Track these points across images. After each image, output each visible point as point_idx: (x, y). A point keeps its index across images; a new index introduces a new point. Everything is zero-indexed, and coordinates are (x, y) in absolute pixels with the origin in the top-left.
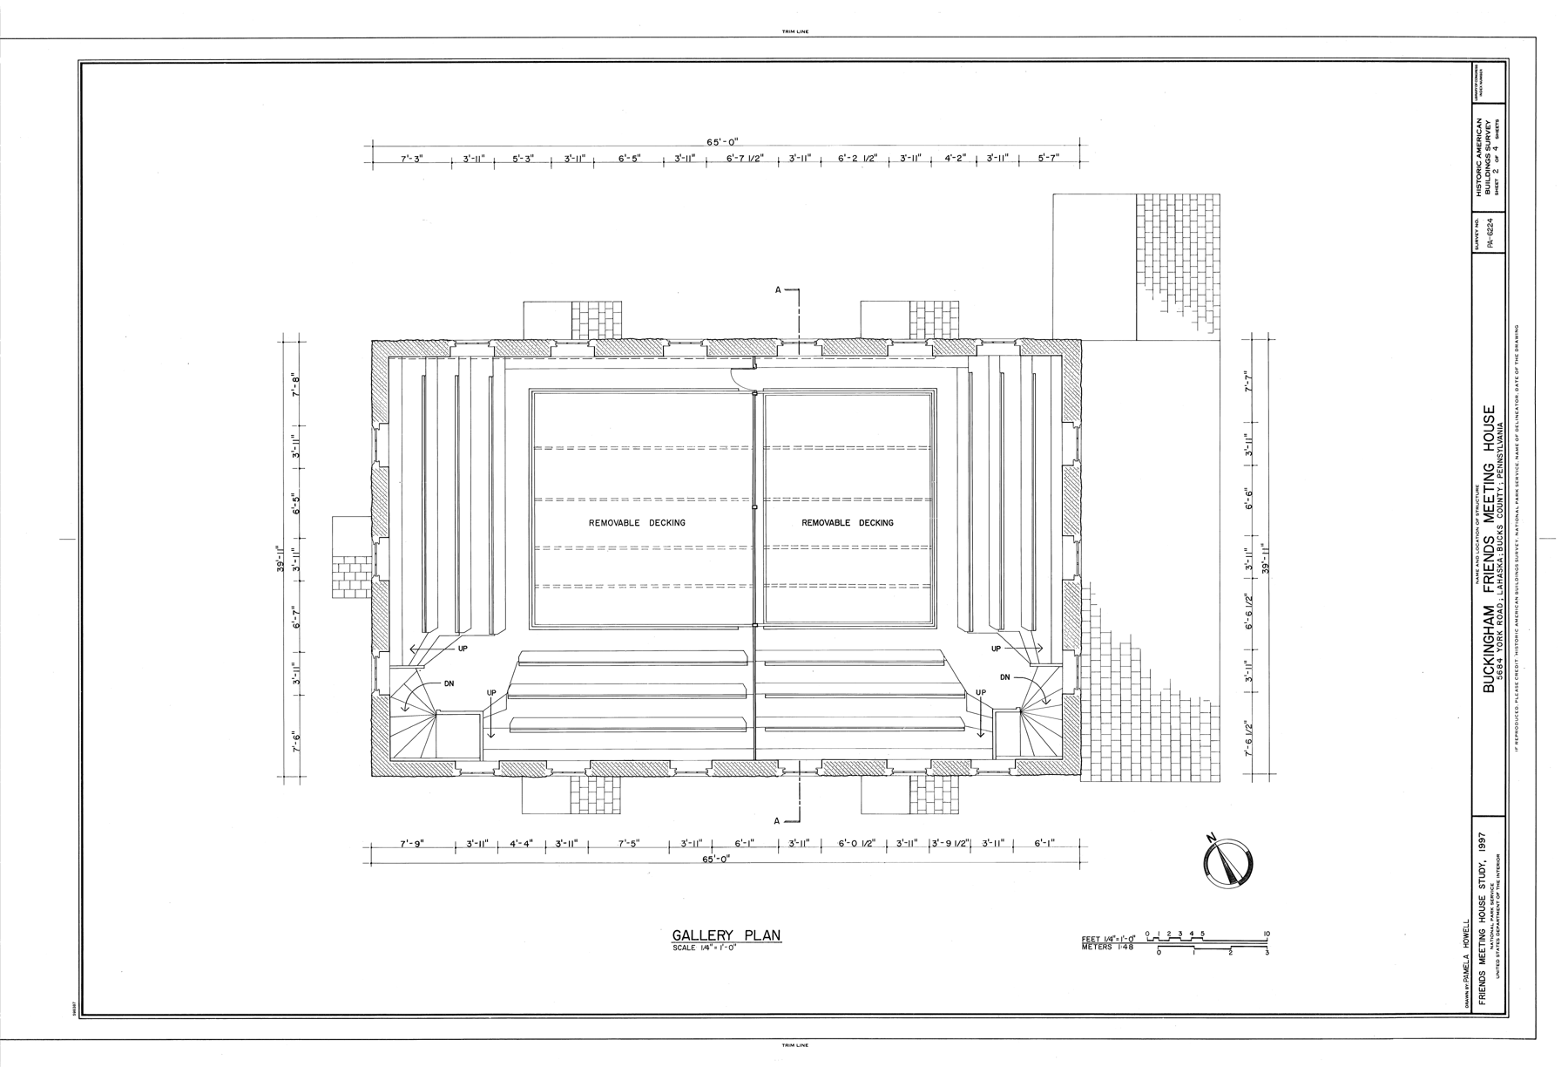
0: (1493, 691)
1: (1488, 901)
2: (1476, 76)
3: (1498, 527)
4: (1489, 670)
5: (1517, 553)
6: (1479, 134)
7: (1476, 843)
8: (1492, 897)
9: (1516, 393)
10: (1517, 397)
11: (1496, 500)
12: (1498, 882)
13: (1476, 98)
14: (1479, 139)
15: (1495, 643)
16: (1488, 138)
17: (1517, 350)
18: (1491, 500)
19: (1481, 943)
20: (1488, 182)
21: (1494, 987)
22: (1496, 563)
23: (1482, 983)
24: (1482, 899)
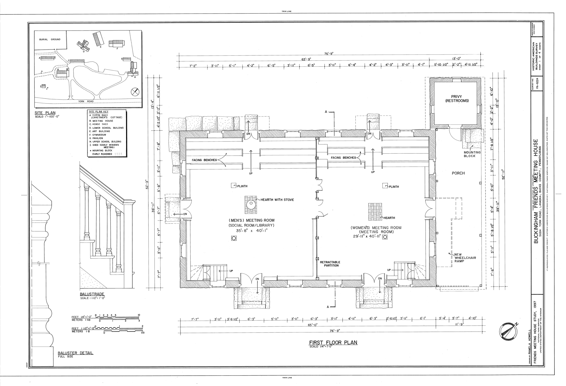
1: (537, 326)
2: (532, 27)
6: (533, 48)
7: (533, 305)
8: (538, 324)
9: (547, 141)
10: (547, 143)
13: (532, 35)
14: (533, 50)
16: (537, 49)
17: (547, 126)
20: (537, 65)
23: (535, 355)
24: (535, 325)
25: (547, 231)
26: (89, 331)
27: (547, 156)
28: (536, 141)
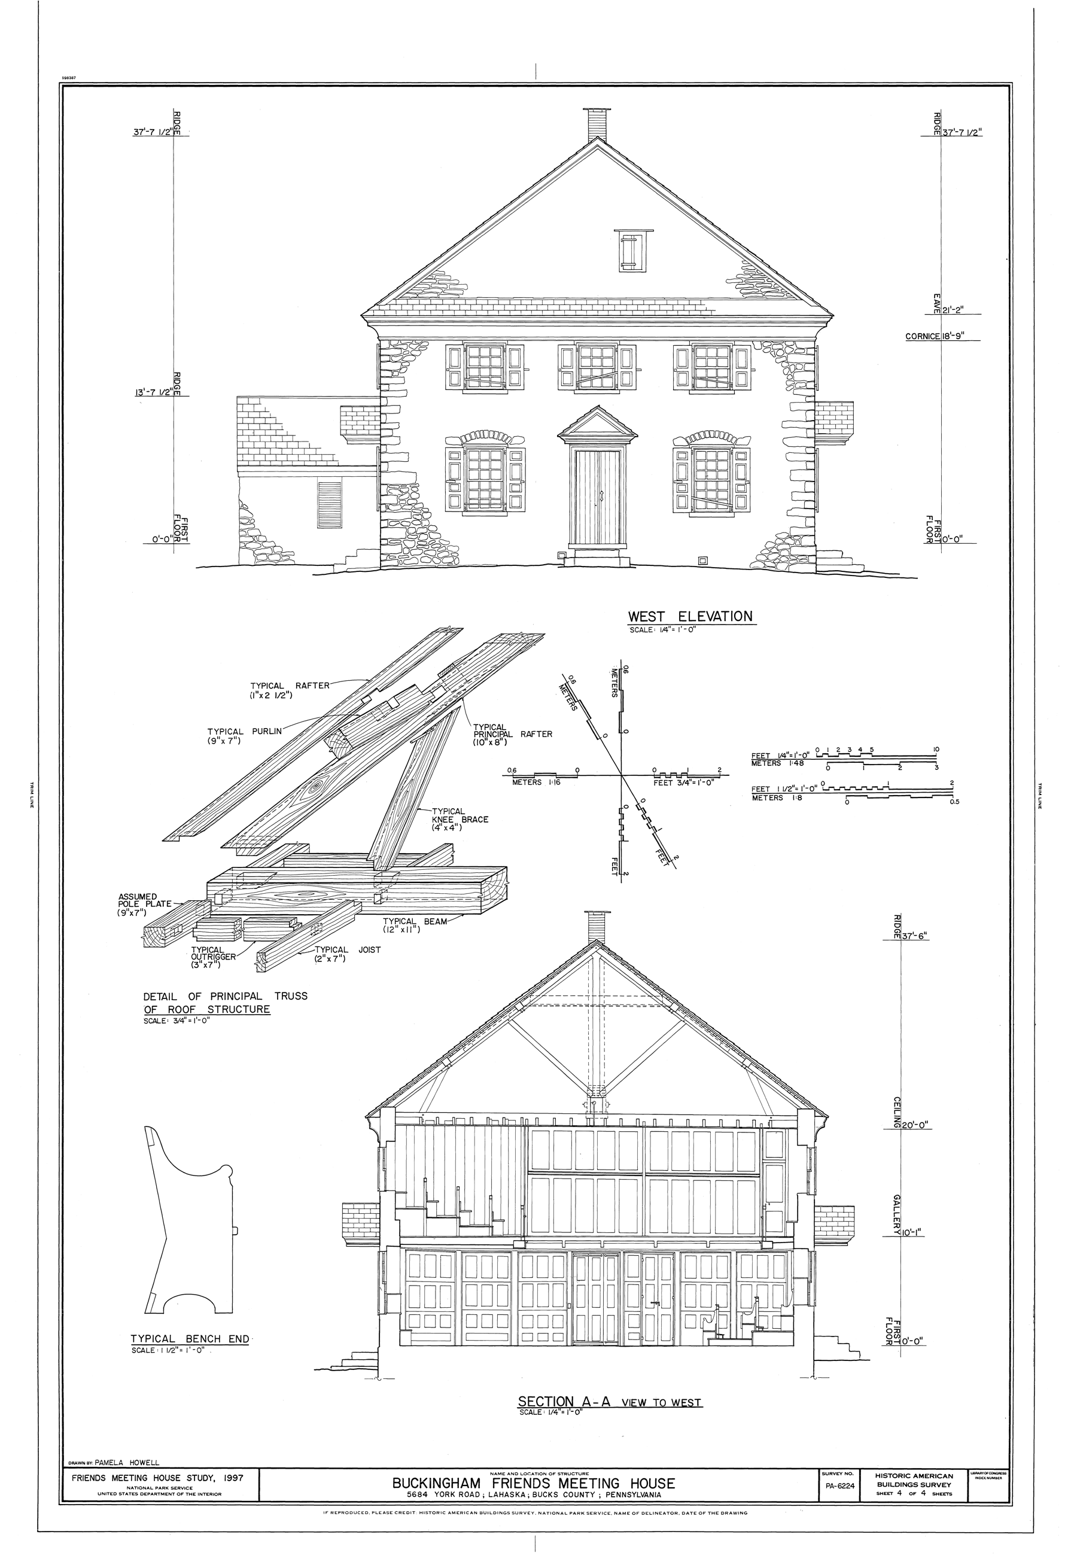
0: (394, 1487)
1: (175, 1484)
2: (995, 1473)
3: (556, 1493)
4: (415, 1483)
5: (521, 1513)
6: (937, 1476)
7: (232, 1472)
8: (179, 1488)
9: (680, 1512)
10: (676, 1513)
11: (582, 1491)
12: (194, 1494)
13: (974, 1473)
14: (932, 1476)
15: (443, 1489)
16: (933, 1485)
17: (722, 1513)
18: (583, 1485)
19: (133, 1477)
20: (889, 1485)
21: (89, 1490)
22: (520, 1491)
23: (94, 1478)
24: (176, 1478)
25: (434, 1513)
26: (800, 798)
27: (640, 1513)
28: (670, 1486)
